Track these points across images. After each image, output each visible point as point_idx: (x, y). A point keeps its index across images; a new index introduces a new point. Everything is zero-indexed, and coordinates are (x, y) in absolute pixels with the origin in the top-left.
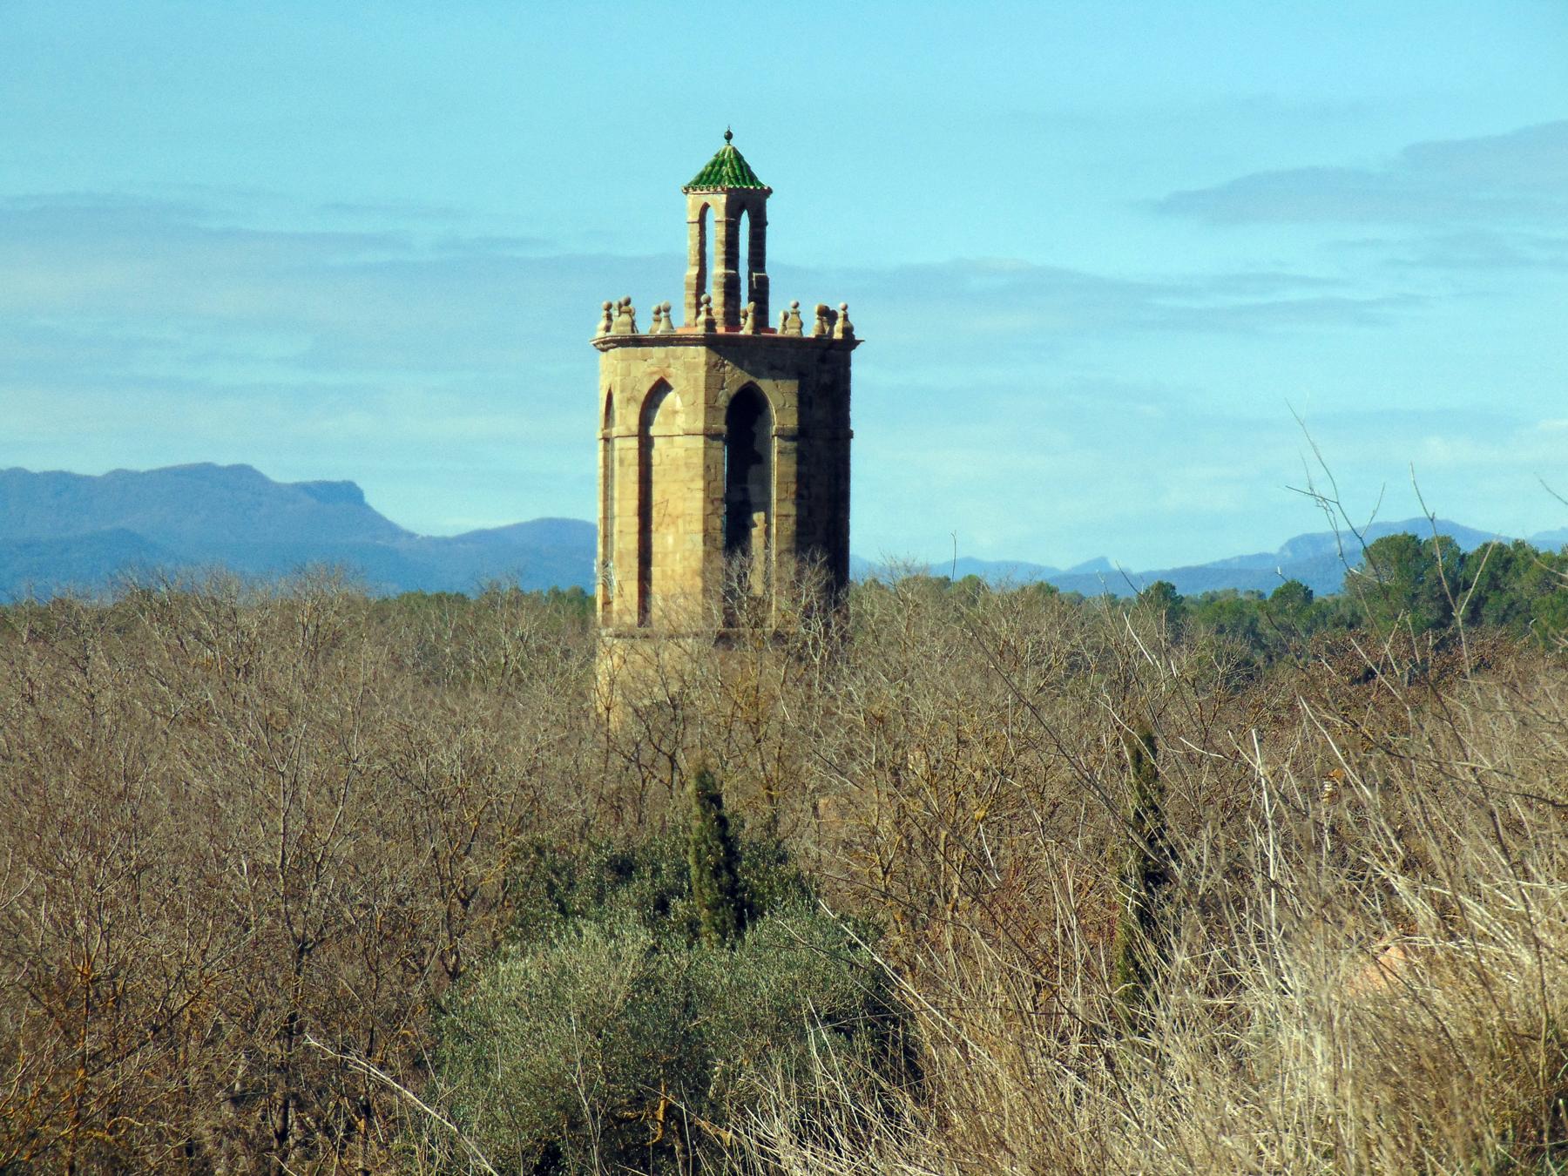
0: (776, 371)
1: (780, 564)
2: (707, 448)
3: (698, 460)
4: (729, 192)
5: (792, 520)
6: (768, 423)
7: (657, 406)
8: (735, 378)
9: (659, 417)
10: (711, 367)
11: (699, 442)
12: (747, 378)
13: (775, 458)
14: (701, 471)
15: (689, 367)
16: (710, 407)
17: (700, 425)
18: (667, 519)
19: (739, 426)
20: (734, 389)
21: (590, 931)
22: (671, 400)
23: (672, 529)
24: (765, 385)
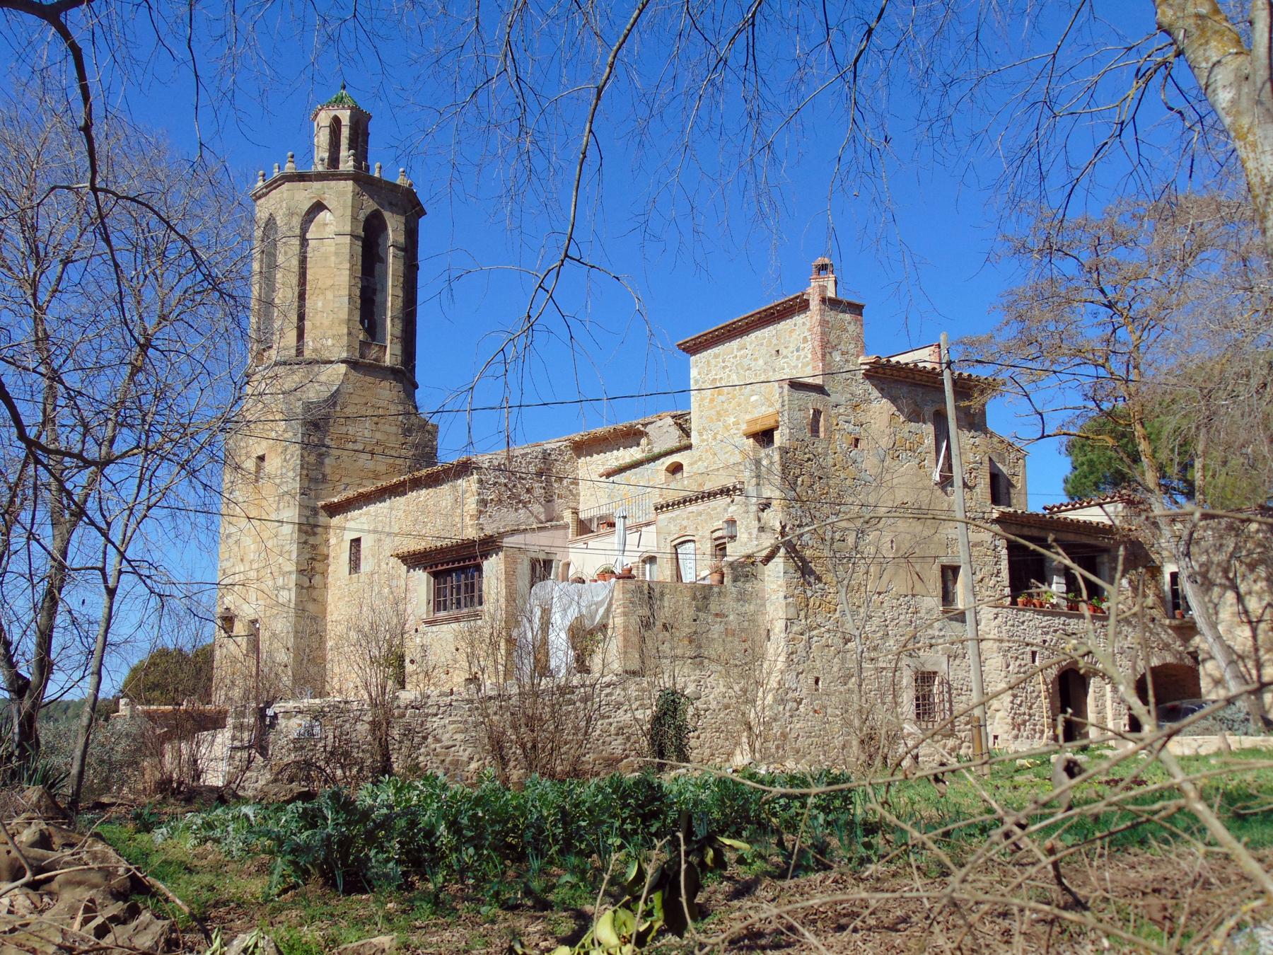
0: (393, 207)
1: (393, 326)
2: (352, 244)
3: (346, 250)
4: (351, 109)
5: (400, 300)
6: (387, 238)
7: (311, 221)
8: (370, 205)
9: (313, 227)
10: (356, 195)
11: (348, 239)
12: (376, 207)
13: (391, 260)
14: (348, 257)
15: (341, 194)
16: (354, 218)
17: (348, 229)
18: (317, 291)
19: (369, 240)
20: (369, 211)
21: (393, 409)
22: (324, 216)
23: (321, 297)
24: (387, 215)
